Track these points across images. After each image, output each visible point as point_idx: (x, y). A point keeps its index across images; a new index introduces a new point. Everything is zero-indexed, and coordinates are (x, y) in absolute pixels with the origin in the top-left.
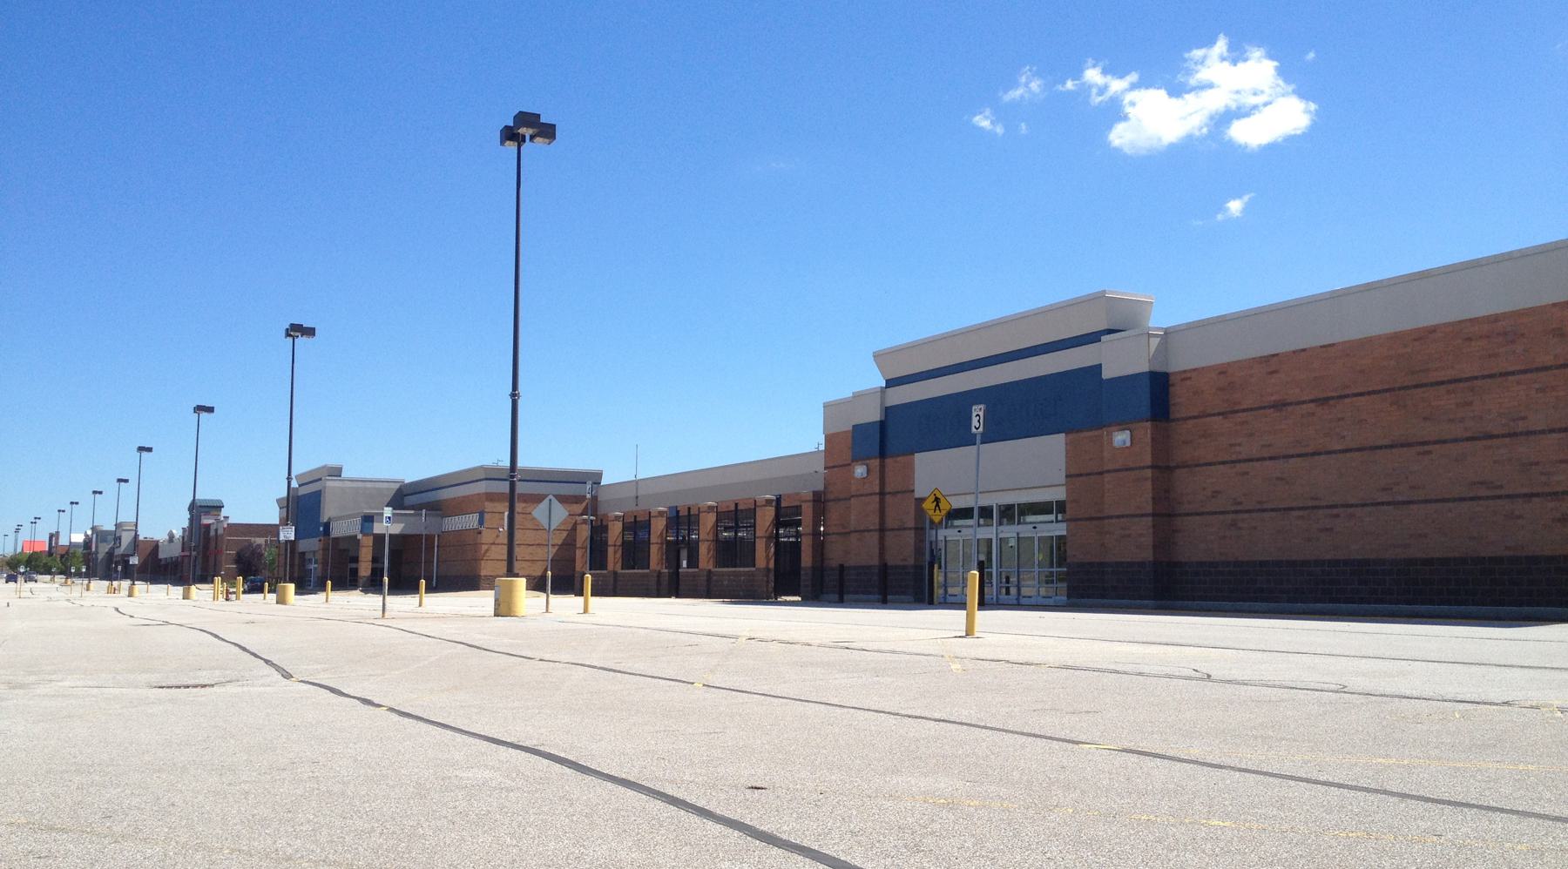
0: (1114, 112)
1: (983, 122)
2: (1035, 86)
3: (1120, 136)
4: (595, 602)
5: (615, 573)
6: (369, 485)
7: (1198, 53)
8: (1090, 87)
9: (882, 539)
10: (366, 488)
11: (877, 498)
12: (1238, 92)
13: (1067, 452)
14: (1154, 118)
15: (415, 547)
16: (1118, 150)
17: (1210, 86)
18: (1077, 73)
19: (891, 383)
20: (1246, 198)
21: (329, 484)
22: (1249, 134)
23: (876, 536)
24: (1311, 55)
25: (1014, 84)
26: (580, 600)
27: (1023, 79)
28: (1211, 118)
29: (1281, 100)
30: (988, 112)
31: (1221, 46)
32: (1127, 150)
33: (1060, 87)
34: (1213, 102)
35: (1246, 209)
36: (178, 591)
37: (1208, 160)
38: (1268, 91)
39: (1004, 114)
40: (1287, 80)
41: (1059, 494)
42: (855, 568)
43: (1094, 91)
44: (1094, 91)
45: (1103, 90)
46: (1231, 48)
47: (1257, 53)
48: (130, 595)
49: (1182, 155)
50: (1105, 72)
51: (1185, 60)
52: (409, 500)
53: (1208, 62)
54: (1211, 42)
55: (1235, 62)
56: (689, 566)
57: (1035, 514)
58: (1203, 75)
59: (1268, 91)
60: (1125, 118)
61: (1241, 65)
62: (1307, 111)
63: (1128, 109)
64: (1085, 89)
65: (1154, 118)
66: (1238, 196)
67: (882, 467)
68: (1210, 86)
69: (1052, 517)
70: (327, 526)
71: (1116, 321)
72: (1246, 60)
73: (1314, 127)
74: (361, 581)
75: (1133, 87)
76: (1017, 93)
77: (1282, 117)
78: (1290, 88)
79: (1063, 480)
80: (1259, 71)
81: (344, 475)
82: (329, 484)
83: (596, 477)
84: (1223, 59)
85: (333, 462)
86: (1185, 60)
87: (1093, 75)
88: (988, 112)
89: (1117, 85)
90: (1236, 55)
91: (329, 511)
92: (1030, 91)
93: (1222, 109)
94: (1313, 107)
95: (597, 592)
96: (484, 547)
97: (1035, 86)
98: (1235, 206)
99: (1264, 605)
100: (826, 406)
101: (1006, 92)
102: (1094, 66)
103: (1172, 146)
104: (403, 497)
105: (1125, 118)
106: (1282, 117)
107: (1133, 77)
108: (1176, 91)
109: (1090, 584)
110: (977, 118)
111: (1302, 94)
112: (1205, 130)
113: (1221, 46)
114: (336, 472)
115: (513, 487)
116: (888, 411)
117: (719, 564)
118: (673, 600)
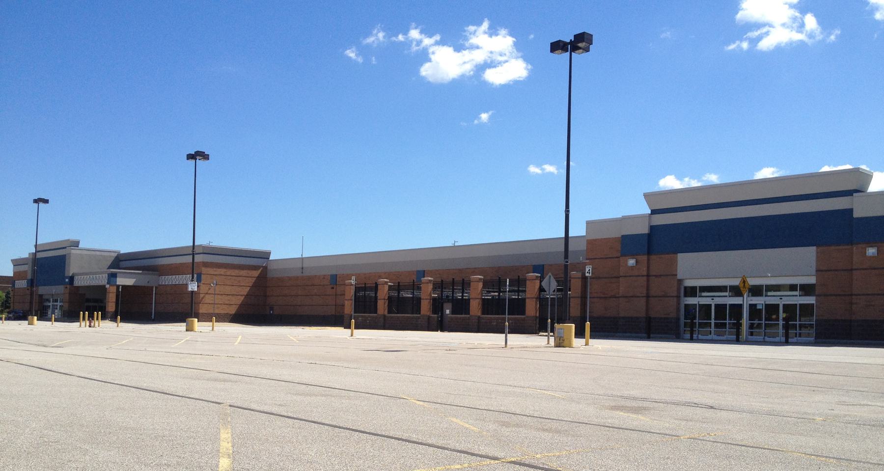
0: (424, 56)
1: (351, 54)
2: (381, 35)
3: (426, 70)
4: (591, 341)
5: (384, 316)
6: (98, 253)
7: (472, 28)
8: (411, 42)
9: (647, 302)
10: (95, 255)
11: (645, 278)
12: (491, 52)
13: (817, 257)
14: (446, 63)
15: (148, 293)
16: (423, 78)
17: (478, 47)
18: (406, 32)
19: (654, 212)
20: (490, 113)
21: (73, 251)
22: (495, 77)
23: (643, 300)
24: (532, 36)
25: (368, 34)
26: (349, 331)
27: (375, 32)
28: (476, 66)
29: (513, 61)
30: (354, 49)
31: (485, 25)
32: (431, 80)
33: (394, 39)
34: (479, 57)
35: (490, 118)
36: (182, 326)
37: (472, 89)
38: (508, 54)
39: (364, 51)
40: (518, 50)
41: (812, 280)
42: (623, 318)
43: (414, 43)
44: (414, 43)
45: (419, 42)
46: (490, 27)
47: (503, 32)
48: (90, 326)
49: (458, 85)
50: (421, 33)
51: (465, 31)
52: (122, 264)
53: (477, 33)
54: (479, 24)
55: (491, 36)
56: (453, 312)
57: (709, 292)
58: (474, 41)
59: (508, 54)
60: (430, 60)
61: (494, 37)
62: (526, 69)
63: (432, 57)
64: (408, 44)
65: (446, 63)
66: (486, 111)
67: (648, 260)
68: (478, 47)
69: (727, 294)
70: (72, 279)
71: (854, 184)
72: (497, 35)
73: (529, 78)
74: (109, 315)
75: (437, 43)
76: (370, 40)
77: (514, 70)
78: (520, 54)
79: (814, 272)
80: (504, 42)
81: (81, 246)
82: (73, 251)
83: (265, 255)
84: (485, 33)
85: (73, 237)
86: (465, 31)
87: (414, 34)
88: (354, 49)
89: (427, 41)
90: (493, 32)
91: (72, 269)
92: (378, 39)
93: (482, 62)
94: (530, 67)
95: (356, 328)
96: (202, 296)
97: (381, 35)
98: (484, 116)
99: (874, 342)
100: (588, 223)
101: (365, 38)
102: (416, 28)
103: (454, 81)
104: (120, 261)
105: (430, 60)
106: (514, 70)
107: (437, 37)
108: (458, 48)
109: (833, 333)
110: (348, 51)
111: (526, 59)
112: (472, 73)
113: (485, 25)
114: (76, 244)
115: (199, 261)
116: (652, 228)
117: (483, 313)
118: (439, 333)
